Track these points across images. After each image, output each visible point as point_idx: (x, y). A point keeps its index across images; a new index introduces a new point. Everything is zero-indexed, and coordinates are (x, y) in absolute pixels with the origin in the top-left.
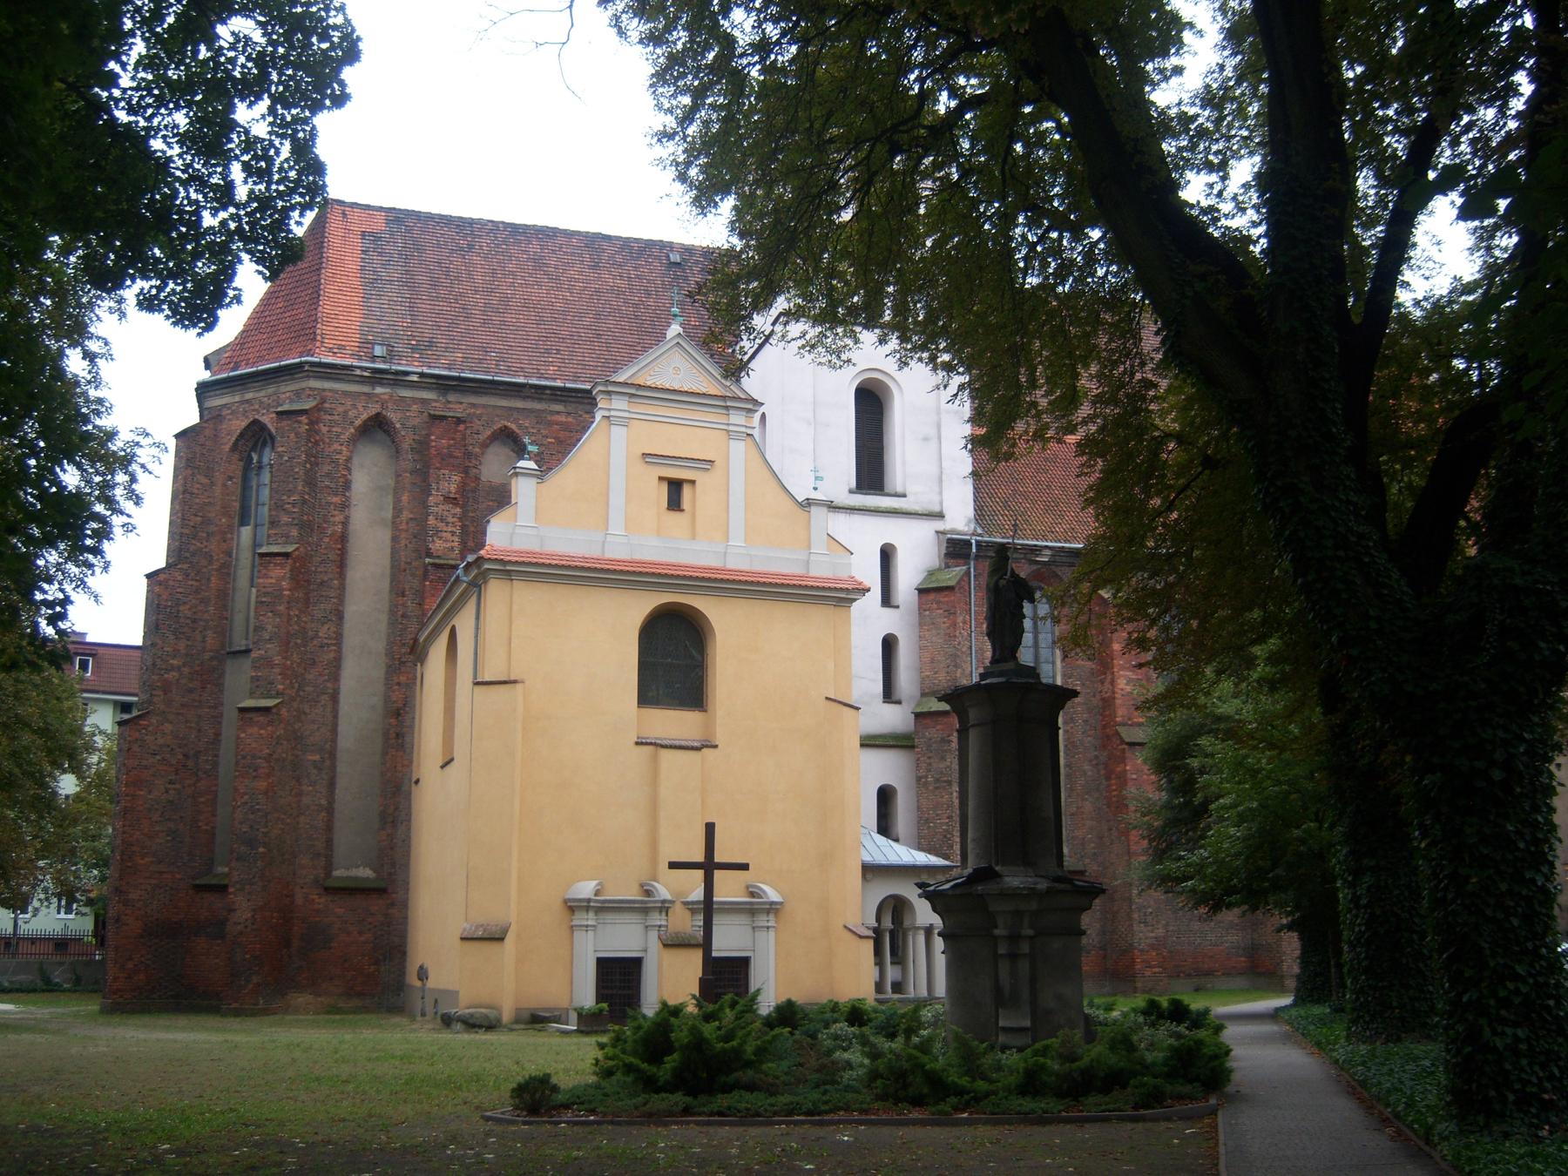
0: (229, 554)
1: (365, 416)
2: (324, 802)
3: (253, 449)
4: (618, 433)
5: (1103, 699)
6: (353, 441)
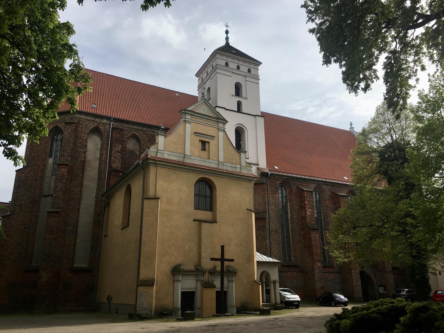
0: (45, 166)
1: (92, 127)
2: (73, 243)
3: (55, 135)
4: (188, 125)
5: (302, 217)
6: (88, 134)
